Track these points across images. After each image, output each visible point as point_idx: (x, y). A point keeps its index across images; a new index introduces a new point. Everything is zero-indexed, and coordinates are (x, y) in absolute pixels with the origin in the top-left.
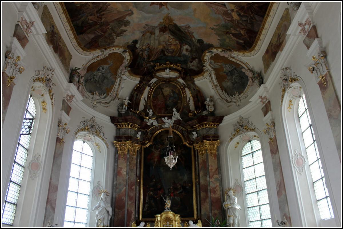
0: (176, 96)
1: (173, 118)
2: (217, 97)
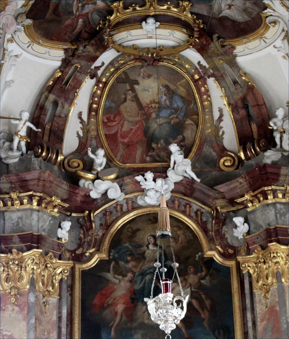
0: (178, 103)
1: (170, 173)
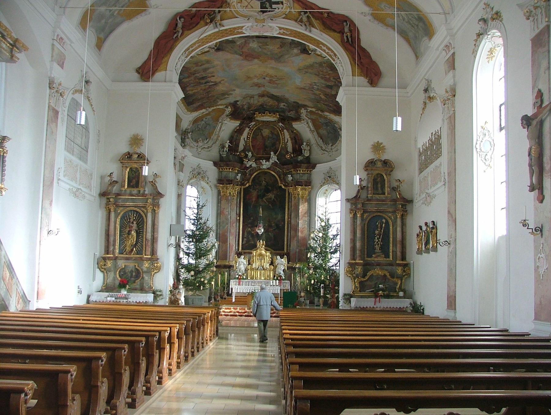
0: (275, 137)
1: (270, 160)
2: (313, 141)
